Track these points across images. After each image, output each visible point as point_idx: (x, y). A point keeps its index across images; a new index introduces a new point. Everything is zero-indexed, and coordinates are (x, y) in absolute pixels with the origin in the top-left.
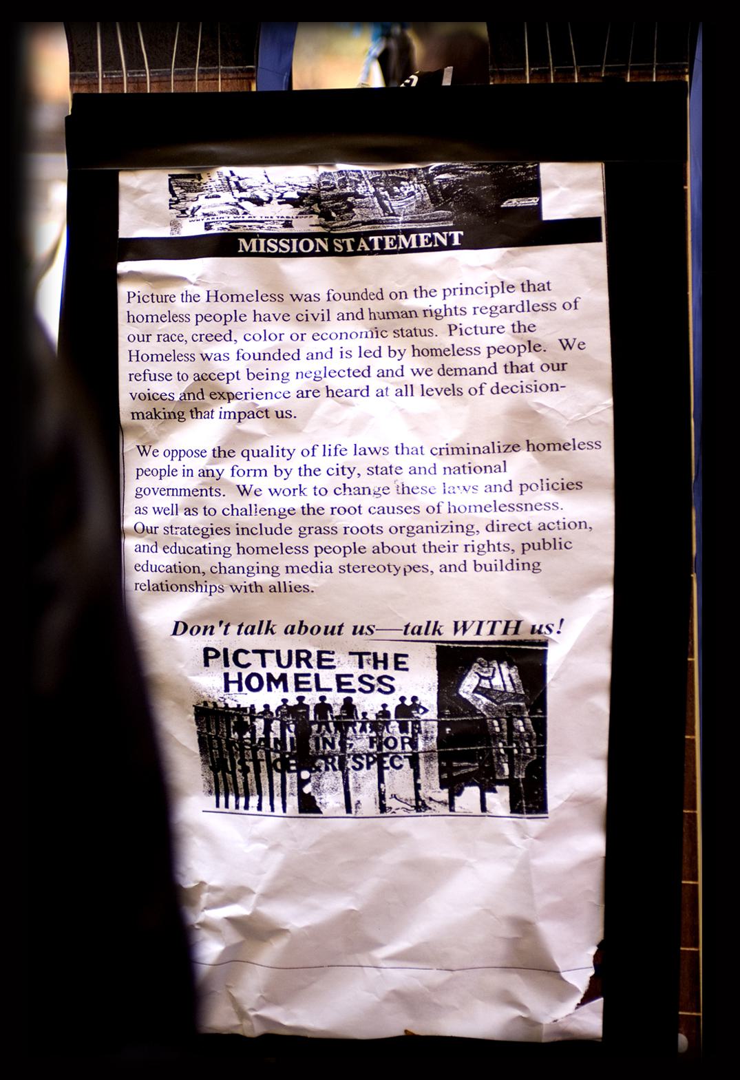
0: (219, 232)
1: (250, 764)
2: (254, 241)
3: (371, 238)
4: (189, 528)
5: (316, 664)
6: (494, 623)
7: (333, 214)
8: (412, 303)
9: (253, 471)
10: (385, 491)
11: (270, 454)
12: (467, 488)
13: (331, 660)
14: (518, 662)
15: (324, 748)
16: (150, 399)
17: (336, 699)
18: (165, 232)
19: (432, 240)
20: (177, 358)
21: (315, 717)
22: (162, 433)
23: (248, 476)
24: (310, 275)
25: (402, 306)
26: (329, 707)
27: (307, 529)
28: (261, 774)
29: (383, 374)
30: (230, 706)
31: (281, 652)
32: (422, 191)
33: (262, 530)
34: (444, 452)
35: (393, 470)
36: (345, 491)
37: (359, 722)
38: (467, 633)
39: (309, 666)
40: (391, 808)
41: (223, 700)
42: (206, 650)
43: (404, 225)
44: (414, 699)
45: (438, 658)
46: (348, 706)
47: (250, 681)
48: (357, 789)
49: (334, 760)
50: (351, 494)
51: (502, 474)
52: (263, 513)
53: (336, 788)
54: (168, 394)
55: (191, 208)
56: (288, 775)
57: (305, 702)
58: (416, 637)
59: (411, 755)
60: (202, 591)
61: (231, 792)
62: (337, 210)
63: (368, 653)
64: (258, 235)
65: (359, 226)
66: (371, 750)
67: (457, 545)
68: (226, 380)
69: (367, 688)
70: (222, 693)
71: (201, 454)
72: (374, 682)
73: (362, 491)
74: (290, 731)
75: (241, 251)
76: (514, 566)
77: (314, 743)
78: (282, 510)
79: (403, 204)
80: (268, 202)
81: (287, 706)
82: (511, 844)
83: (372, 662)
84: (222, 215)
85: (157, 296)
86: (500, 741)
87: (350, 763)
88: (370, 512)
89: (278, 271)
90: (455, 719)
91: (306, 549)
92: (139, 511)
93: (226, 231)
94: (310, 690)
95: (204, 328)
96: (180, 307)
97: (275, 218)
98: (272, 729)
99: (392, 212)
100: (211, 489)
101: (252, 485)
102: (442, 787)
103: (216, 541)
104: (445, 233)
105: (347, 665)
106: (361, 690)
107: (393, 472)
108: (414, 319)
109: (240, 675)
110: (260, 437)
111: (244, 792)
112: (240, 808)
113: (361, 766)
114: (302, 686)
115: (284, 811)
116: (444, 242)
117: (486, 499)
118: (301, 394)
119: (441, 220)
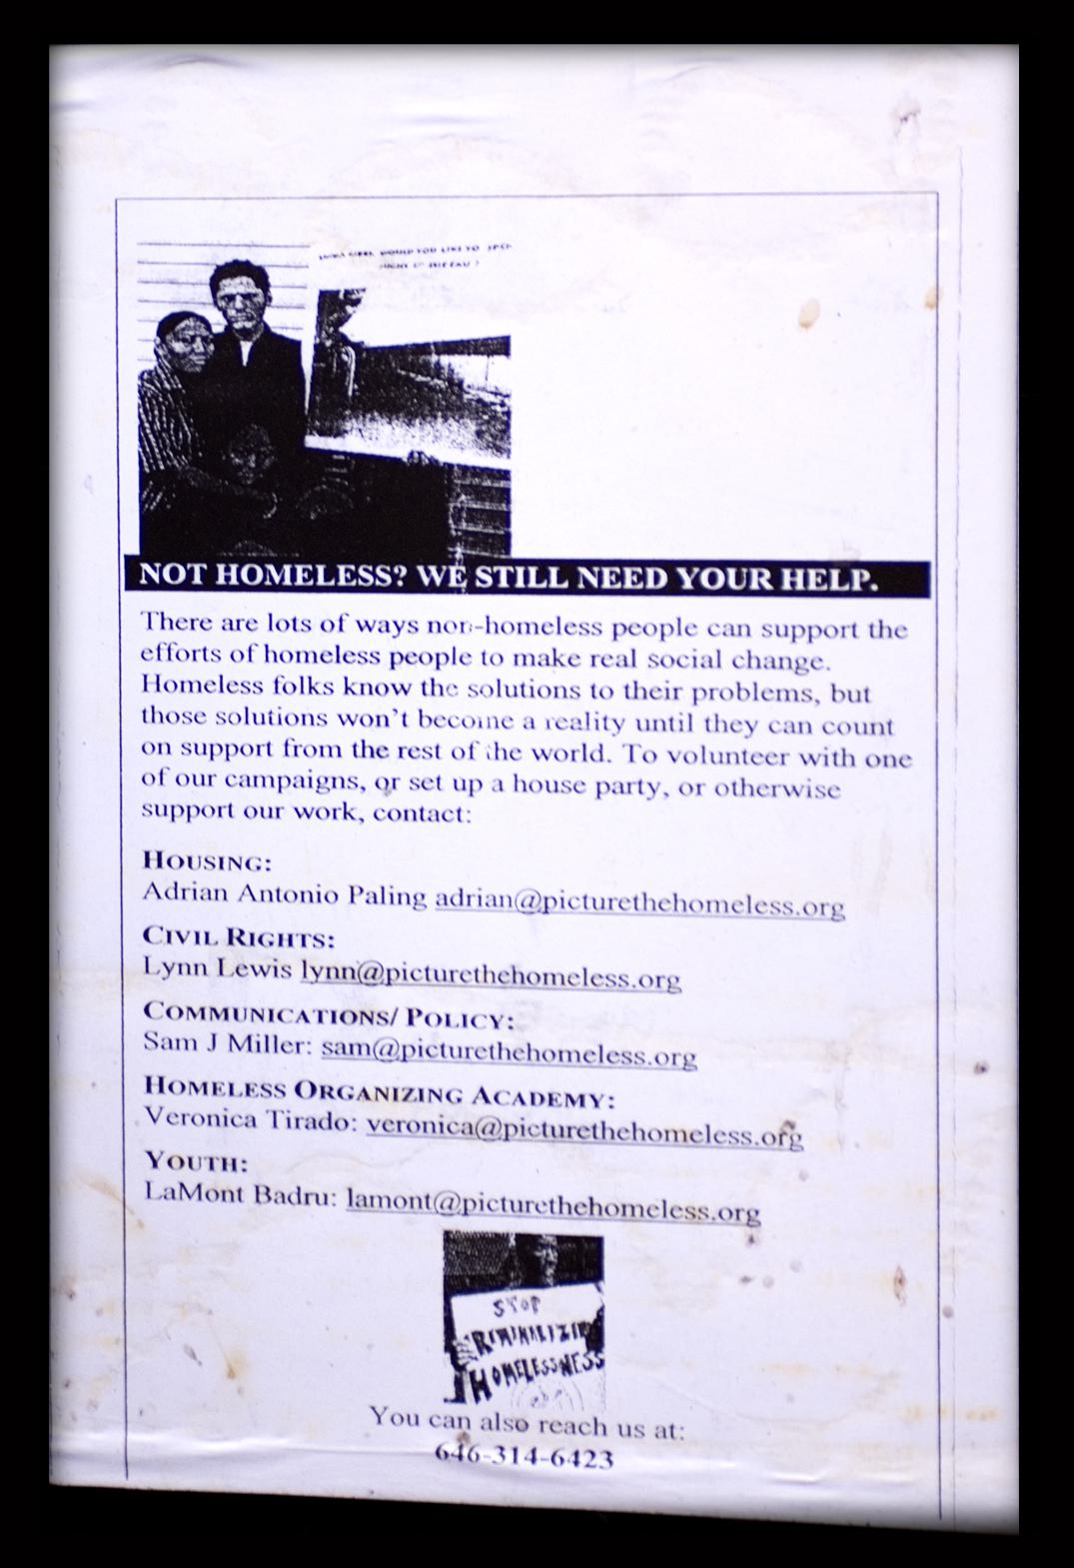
104: (596, 569)
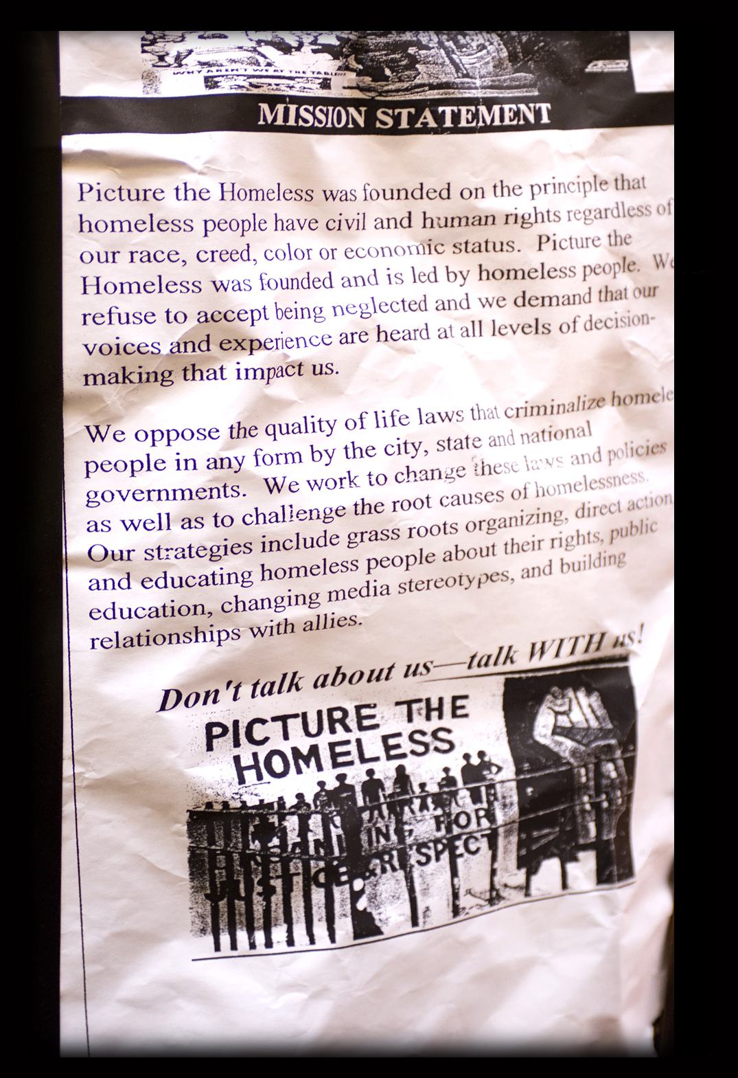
0: (234, 91)
1: (278, 884)
2: (280, 108)
3: (441, 109)
4: (190, 547)
5: (356, 725)
6: (577, 639)
7: (388, 72)
8: (491, 204)
9: (284, 456)
10: (460, 473)
11: (303, 429)
12: (550, 461)
13: (373, 717)
14: (599, 685)
15: (378, 841)
16: (118, 353)
17: (385, 771)
18: (135, 90)
19: (517, 114)
20: (163, 286)
21: (365, 802)
22: (130, 406)
23: (278, 463)
24: (345, 159)
25: (476, 208)
26: (379, 784)
27: (359, 535)
28: (293, 894)
29: (443, 306)
30: (249, 804)
31: (308, 715)
32: (495, 43)
33: (300, 542)
34: (522, 412)
35: (470, 442)
36: (408, 477)
37: (417, 797)
38: (545, 657)
39: (347, 729)
40: (464, 909)
41: (238, 796)
42: (210, 726)
43: (484, 91)
44: (481, 754)
45: (506, 695)
46: (402, 778)
47: (271, 763)
48: (425, 891)
49: (391, 857)
50: (416, 480)
51: (588, 438)
52: (301, 517)
53: (397, 895)
54: (150, 344)
55: (173, 53)
56: (337, 891)
57: (348, 782)
58: (483, 670)
59: (488, 832)
60: (205, 641)
61: (238, 926)
62: (393, 65)
63: (419, 701)
64: (288, 99)
65: (424, 91)
66: (439, 835)
67: (134, 550)
68: (250, 320)
69: (421, 749)
70: (236, 787)
71: (210, 435)
72: (428, 739)
73: (431, 475)
74: (336, 827)
75: (261, 122)
76: (604, 560)
77: (366, 838)
78: (328, 511)
79: (474, 61)
80: (299, 49)
81: (326, 791)
82: (596, 924)
83: (424, 712)
84: (234, 66)
85: (129, 191)
86: (585, 794)
87: (414, 857)
88: (441, 504)
89: (311, 154)
90: (537, 775)
91: (355, 564)
92: (94, 527)
93: (244, 91)
94: (351, 763)
95: (218, 241)
96: (171, 208)
97: (309, 74)
98: (311, 828)
99: (465, 72)
100: (225, 487)
101: (284, 477)
102: (519, 867)
103: (231, 564)
104: (532, 105)
105: (392, 720)
106: (413, 752)
107: (470, 445)
108: (490, 227)
109: (255, 755)
110: (290, 403)
111: (264, 922)
112: (258, 947)
113: (429, 858)
114: (340, 760)
115: (333, 940)
116: (531, 118)
117: (574, 474)
118: (346, 339)
119: (524, 86)
